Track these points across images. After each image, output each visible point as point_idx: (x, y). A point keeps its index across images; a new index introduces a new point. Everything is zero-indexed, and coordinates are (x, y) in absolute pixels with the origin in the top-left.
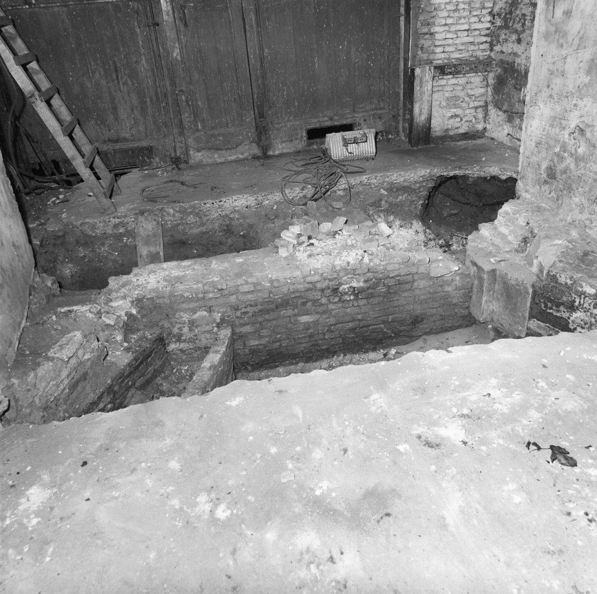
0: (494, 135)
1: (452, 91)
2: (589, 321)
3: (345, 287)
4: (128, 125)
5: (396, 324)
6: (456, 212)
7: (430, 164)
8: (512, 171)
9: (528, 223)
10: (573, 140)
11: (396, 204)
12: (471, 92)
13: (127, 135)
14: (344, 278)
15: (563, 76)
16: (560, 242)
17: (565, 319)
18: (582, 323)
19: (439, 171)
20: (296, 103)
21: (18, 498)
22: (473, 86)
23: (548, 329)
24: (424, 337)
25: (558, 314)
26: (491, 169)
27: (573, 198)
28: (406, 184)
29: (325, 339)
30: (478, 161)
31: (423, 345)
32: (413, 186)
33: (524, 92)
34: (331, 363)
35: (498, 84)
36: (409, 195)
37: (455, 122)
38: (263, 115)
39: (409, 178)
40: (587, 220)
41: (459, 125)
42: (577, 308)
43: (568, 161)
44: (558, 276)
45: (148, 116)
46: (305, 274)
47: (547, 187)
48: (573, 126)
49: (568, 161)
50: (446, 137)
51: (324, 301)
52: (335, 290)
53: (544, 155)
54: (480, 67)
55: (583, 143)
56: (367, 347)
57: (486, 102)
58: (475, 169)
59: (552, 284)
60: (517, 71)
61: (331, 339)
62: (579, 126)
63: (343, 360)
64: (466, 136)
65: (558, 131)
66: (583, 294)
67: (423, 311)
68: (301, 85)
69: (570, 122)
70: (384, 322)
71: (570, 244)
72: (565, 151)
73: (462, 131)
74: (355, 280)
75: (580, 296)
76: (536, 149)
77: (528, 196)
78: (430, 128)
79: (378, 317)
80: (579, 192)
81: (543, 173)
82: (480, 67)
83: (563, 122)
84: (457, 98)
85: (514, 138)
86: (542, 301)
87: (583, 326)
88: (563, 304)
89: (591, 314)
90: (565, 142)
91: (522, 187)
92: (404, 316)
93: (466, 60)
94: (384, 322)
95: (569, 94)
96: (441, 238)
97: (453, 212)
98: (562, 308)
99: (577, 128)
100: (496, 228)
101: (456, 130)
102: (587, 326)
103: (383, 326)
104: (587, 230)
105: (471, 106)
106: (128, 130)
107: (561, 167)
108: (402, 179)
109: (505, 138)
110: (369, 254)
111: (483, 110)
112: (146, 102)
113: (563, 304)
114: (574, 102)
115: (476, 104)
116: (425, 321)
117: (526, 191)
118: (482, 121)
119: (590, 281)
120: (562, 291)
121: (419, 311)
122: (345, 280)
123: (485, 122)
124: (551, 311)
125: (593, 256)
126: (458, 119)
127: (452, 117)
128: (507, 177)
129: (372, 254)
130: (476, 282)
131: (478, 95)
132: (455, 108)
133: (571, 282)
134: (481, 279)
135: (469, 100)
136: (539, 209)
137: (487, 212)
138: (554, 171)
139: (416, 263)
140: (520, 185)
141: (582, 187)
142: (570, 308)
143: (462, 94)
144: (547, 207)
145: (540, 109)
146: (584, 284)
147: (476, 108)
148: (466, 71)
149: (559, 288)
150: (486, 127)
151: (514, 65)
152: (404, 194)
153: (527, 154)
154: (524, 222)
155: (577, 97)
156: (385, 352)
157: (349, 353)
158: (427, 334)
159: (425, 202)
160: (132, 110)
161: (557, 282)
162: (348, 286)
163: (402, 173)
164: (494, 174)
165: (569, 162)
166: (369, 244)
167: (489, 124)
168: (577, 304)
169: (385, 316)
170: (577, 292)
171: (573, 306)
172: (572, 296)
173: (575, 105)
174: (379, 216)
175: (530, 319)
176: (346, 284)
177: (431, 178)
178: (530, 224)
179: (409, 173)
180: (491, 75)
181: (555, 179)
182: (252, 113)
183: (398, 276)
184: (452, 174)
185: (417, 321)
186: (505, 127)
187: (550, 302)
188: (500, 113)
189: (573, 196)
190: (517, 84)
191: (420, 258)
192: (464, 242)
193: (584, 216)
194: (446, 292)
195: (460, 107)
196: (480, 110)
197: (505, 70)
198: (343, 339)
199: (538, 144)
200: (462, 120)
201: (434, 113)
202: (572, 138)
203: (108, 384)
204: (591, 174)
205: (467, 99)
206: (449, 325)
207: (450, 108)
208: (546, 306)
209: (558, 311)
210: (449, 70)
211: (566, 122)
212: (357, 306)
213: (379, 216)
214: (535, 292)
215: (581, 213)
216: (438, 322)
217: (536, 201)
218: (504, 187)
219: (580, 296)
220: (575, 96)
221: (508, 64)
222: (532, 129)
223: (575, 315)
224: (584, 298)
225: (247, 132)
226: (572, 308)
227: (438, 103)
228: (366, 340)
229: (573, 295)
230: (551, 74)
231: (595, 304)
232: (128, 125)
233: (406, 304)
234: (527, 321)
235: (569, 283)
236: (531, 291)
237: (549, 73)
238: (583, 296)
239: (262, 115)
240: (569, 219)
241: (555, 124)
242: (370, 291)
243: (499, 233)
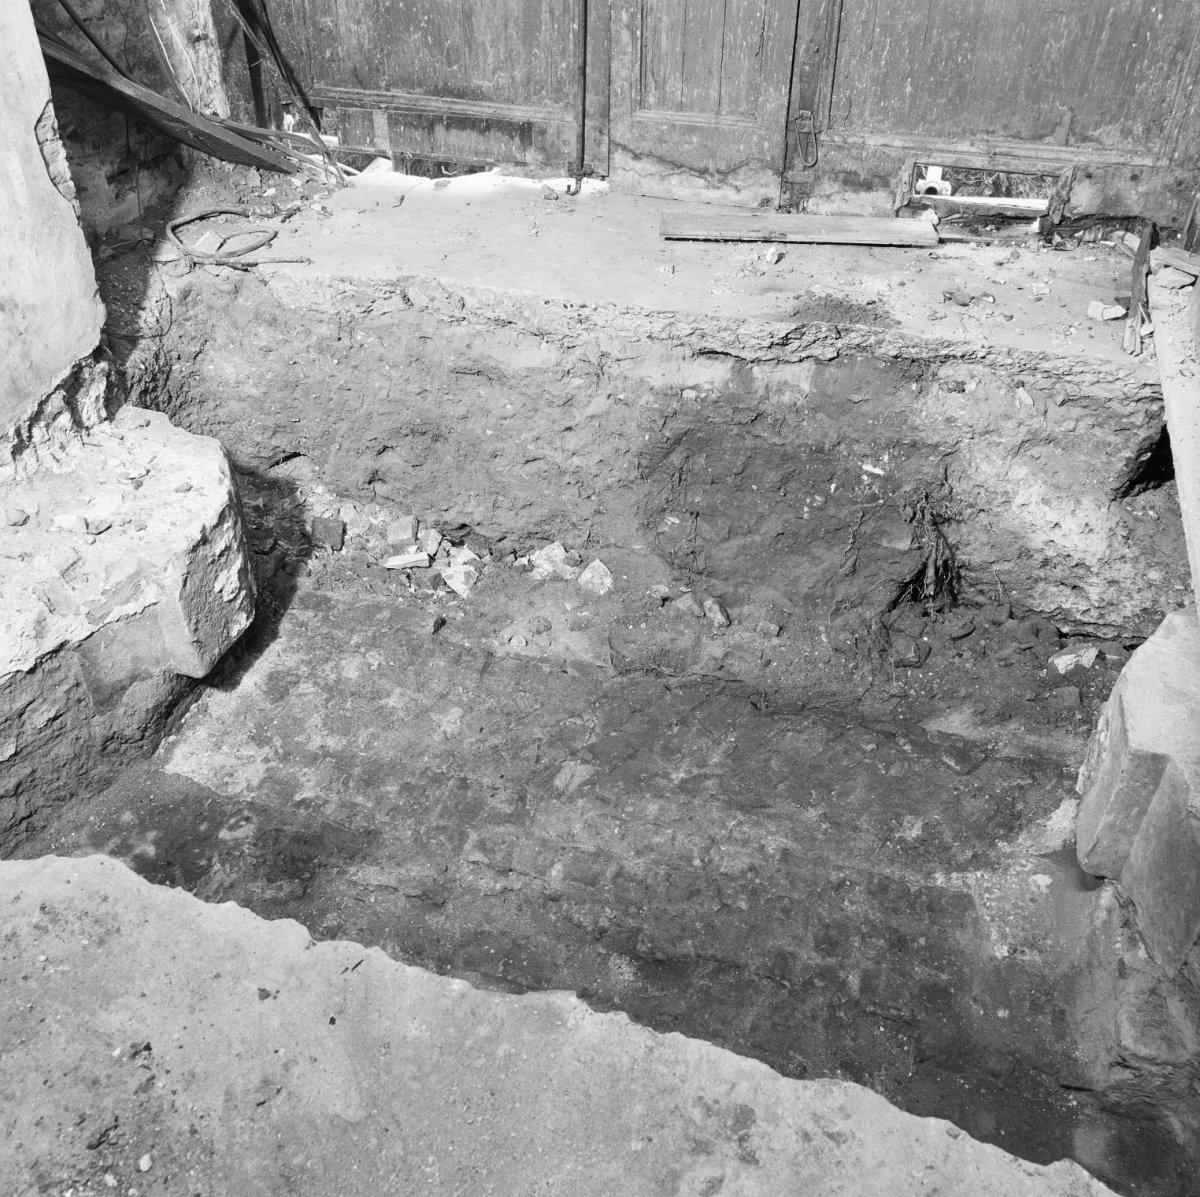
4: (491, 59)
13: (486, 85)
20: (909, 89)
21: (344, 1127)
32: (1114, 405)
38: (812, 101)
45: (538, 46)
46: (13, 800)
68: (934, 41)
106: (489, 74)
112: (538, 13)
160: (506, 26)
182: (785, 90)
203: (683, 520)
225: (762, 138)
232: (491, 59)
239: (807, 103)
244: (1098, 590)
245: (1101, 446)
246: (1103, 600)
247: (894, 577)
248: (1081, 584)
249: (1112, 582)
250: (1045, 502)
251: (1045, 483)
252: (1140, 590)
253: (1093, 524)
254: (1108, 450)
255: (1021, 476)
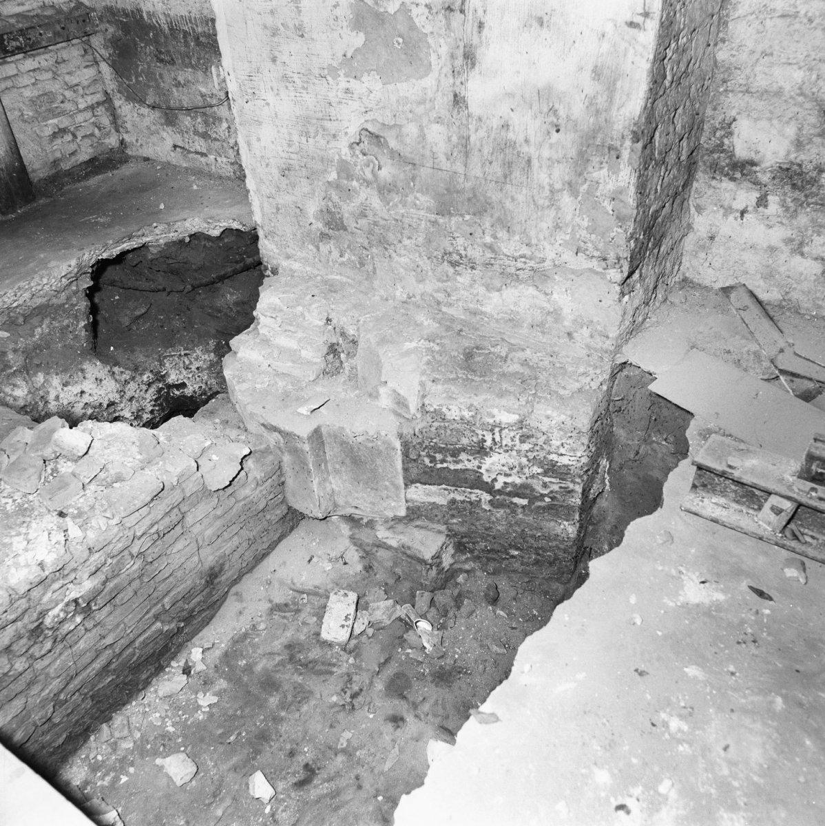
0: (147, 152)
1: (33, 84)
2: (516, 464)
3: (56, 611)
5: (180, 604)
6: (143, 311)
7: (68, 246)
8: (229, 219)
9: (328, 320)
10: (361, 156)
11: (37, 347)
12: (73, 80)
14: (45, 599)
15: (302, 36)
16: (414, 344)
17: (474, 471)
18: (505, 469)
19: (91, 255)
22: (71, 67)
23: (446, 492)
24: (233, 590)
25: (459, 467)
26: (187, 224)
27: (396, 258)
28: (39, 301)
29: (55, 725)
30: (155, 214)
31: (239, 606)
32: (55, 301)
33: (218, 75)
34: (92, 756)
35: (119, 55)
36: (54, 319)
37: (62, 146)
39: (39, 288)
40: (438, 291)
41: (73, 147)
42: (491, 449)
43: (363, 196)
44: (444, 410)
47: (331, 245)
48: (353, 130)
49: (363, 196)
50: (59, 178)
51: (20, 665)
52: (37, 632)
53: (306, 189)
54: (73, 28)
55: (385, 160)
56: (144, 677)
57: (106, 93)
58: (157, 231)
59: (436, 424)
60: (151, 27)
61: (68, 715)
62: (367, 130)
63: (112, 736)
64: (97, 165)
65: (323, 142)
66: (495, 426)
67: (218, 554)
69: (346, 124)
70: (157, 617)
71: (432, 344)
72: (350, 177)
73: (83, 157)
74: (70, 586)
75: (492, 430)
76: (285, 181)
77: (296, 266)
78: (23, 169)
79: (141, 619)
80: (405, 246)
81: (314, 221)
82: (73, 28)
83: (328, 124)
84: (49, 96)
85: (189, 152)
86: (423, 453)
87: (508, 472)
88: (464, 450)
89: (519, 451)
90: (343, 161)
91: (276, 251)
92: (189, 582)
93: (37, 15)
94: (157, 617)
95: (326, 71)
96: (144, 370)
97: (138, 313)
98: (463, 456)
99: (364, 133)
100: (266, 342)
101: (73, 159)
102: (515, 471)
103: (158, 625)
104: (444, 309)
105: (81, 106)
107: (347, 210)
108: (27, 295)
109: (172, 154)
110: (74, 517)
111: (107, 110)
113: (464, 450)
114: (343, 85)
115: (91, 100)
116: (226, 567)
117: (288, 257)
118: (113, 131)
119: (504, 402)
120: (458, 431)
121: (211, 558)
122: (51, 601)
123: (118, 131)
124: (445, 465)
125: (480, 355)
126: (69, 137)
127: (54, 136)
128: (222, 230)
129: (80, 515)
130: (287, 458)
131: (86, 83)
132: (55, 116)
133: (471, 414)
134: (295, 452)
135: (75, 95)
136: (331, 288)
137: (203, 296)
138: (338, 216)
139: (175, 484)
140: (267, 248)
141: (409, 238)
142: (478, 452)
143: (55, 87)
144: (345, 279)
145: (268, 104)
146: (495, 411)
147: (92, 108)
148: (49, 39)
149: (451, 427)
150: (123, 139)
151: (142, 17)
152: (42, 322)
153: (266, 190)
154: (321, 320)
155: (346, 75)
156: (182, 664)
157: (115, 711)
158: (236, 581)
159: (88, 319)
161: (444, 419)
162: (60, 606)
163: (22, 284)
164: (194, 230)
165: (367, 196)
166: (62, 494)
167: (127, 132)
168: (489, 443)
169: (155, 605)
170: (484, 426)
171: (482, 448)
172: (477, 434)
173: (347, 91)
174: (15, 385)
175: (406, 485)
176: (57, 605)
177: (80, 273)
178: (334, 321)
179: (37, 279)
180: (96, 41)
181: (345, 229)
183: (152, 525)
184: (116, 251)
185: (212, 576)
186: (165, 135)
187: (440, 452)
188: (145, 111)
189: (394, 255)
190: (160, 52)
191: (179, 470)
192: (187, 362)
193: (429, 286)
194: (244, 499)
195: (63, 113)
196: (101, 110)
197: (125, 28)
198: (92, 697)
199: (285, 171)
200: (75, 136)
201: (19, 136)
202: (358, 152)
204: (422, 213)
205: (68, 94)
206: (265, 546)
207: (46, 119)
208: (433, 460)
209: (457, 462)
210: (14, 44)
211: (335, 123)
212: (95, 626)
213: (15, 385)
214: (406, 445)
215: (420, 281)
216: (246, 554)
217: (316, 272)
218: (220, 247)
219: (492, 430)
220: (341, 73)
221: (127, 15)
222: (263, 144)
223: (488, 462)
224: (500, 432)
226: (481, 450)
227: (17, 113)
228: (136, 668)
229: (480, 432)
230: (274, 35)
231: (521, 436)
233: (185, 560)
234: (403, 491)
235: (467, 416)
236: (398, 444)
237: (268, 33)
238: (497, 430)
240: (400, 294)
241: (312, 130)
242: (111, 585)
243: (282, 351)
244: (127, 409)
245: (65, 331)
246: (133, 413)
247: (601, 379)
248: (117, 414)
249: (131, 399)
250: (65, 385)
251: (57, 374)
252: (146, 391)
253: (99, 376)
254: (70, 329)
255: (42, 381)
